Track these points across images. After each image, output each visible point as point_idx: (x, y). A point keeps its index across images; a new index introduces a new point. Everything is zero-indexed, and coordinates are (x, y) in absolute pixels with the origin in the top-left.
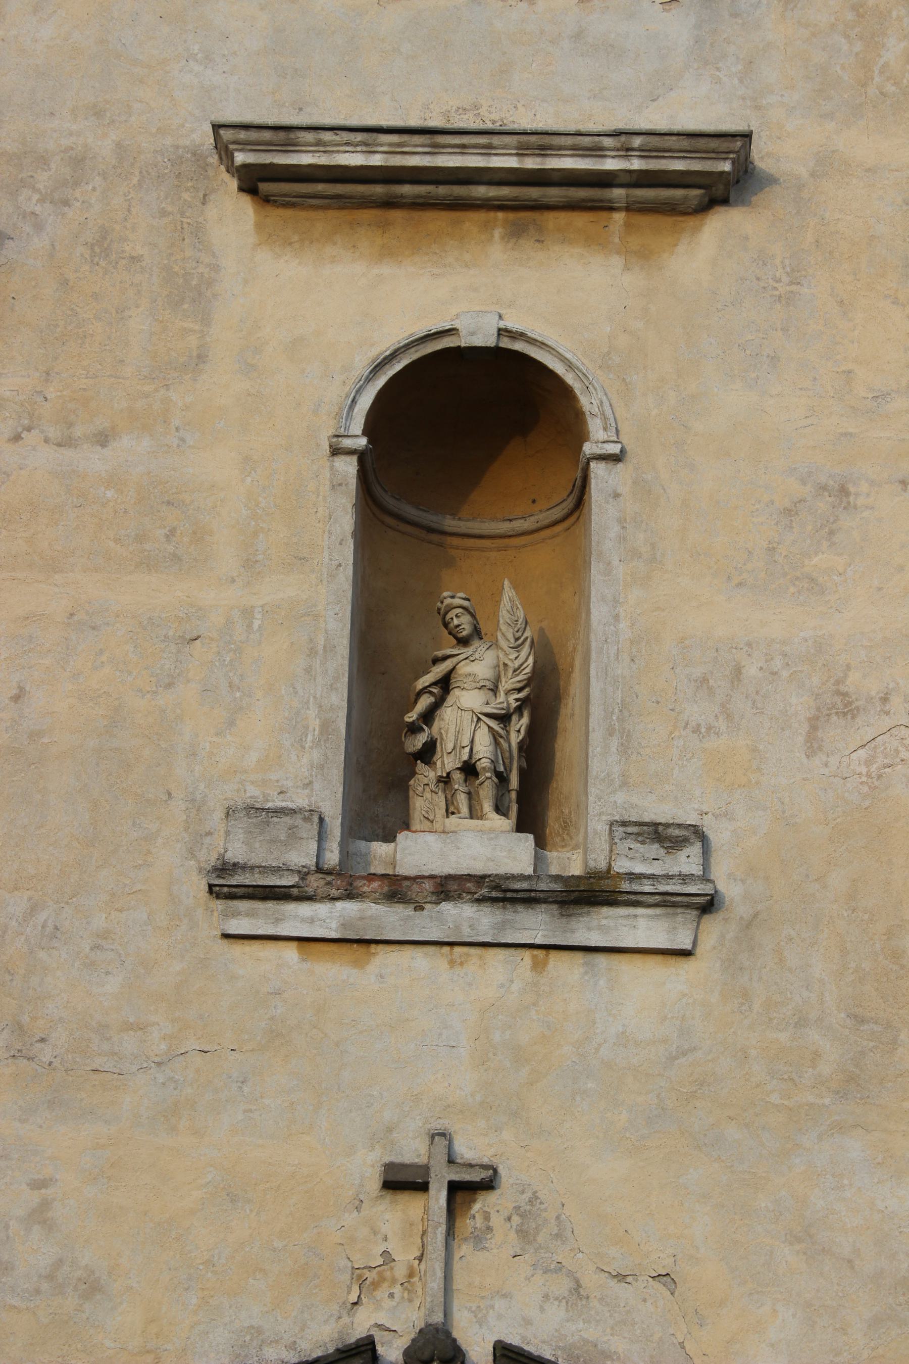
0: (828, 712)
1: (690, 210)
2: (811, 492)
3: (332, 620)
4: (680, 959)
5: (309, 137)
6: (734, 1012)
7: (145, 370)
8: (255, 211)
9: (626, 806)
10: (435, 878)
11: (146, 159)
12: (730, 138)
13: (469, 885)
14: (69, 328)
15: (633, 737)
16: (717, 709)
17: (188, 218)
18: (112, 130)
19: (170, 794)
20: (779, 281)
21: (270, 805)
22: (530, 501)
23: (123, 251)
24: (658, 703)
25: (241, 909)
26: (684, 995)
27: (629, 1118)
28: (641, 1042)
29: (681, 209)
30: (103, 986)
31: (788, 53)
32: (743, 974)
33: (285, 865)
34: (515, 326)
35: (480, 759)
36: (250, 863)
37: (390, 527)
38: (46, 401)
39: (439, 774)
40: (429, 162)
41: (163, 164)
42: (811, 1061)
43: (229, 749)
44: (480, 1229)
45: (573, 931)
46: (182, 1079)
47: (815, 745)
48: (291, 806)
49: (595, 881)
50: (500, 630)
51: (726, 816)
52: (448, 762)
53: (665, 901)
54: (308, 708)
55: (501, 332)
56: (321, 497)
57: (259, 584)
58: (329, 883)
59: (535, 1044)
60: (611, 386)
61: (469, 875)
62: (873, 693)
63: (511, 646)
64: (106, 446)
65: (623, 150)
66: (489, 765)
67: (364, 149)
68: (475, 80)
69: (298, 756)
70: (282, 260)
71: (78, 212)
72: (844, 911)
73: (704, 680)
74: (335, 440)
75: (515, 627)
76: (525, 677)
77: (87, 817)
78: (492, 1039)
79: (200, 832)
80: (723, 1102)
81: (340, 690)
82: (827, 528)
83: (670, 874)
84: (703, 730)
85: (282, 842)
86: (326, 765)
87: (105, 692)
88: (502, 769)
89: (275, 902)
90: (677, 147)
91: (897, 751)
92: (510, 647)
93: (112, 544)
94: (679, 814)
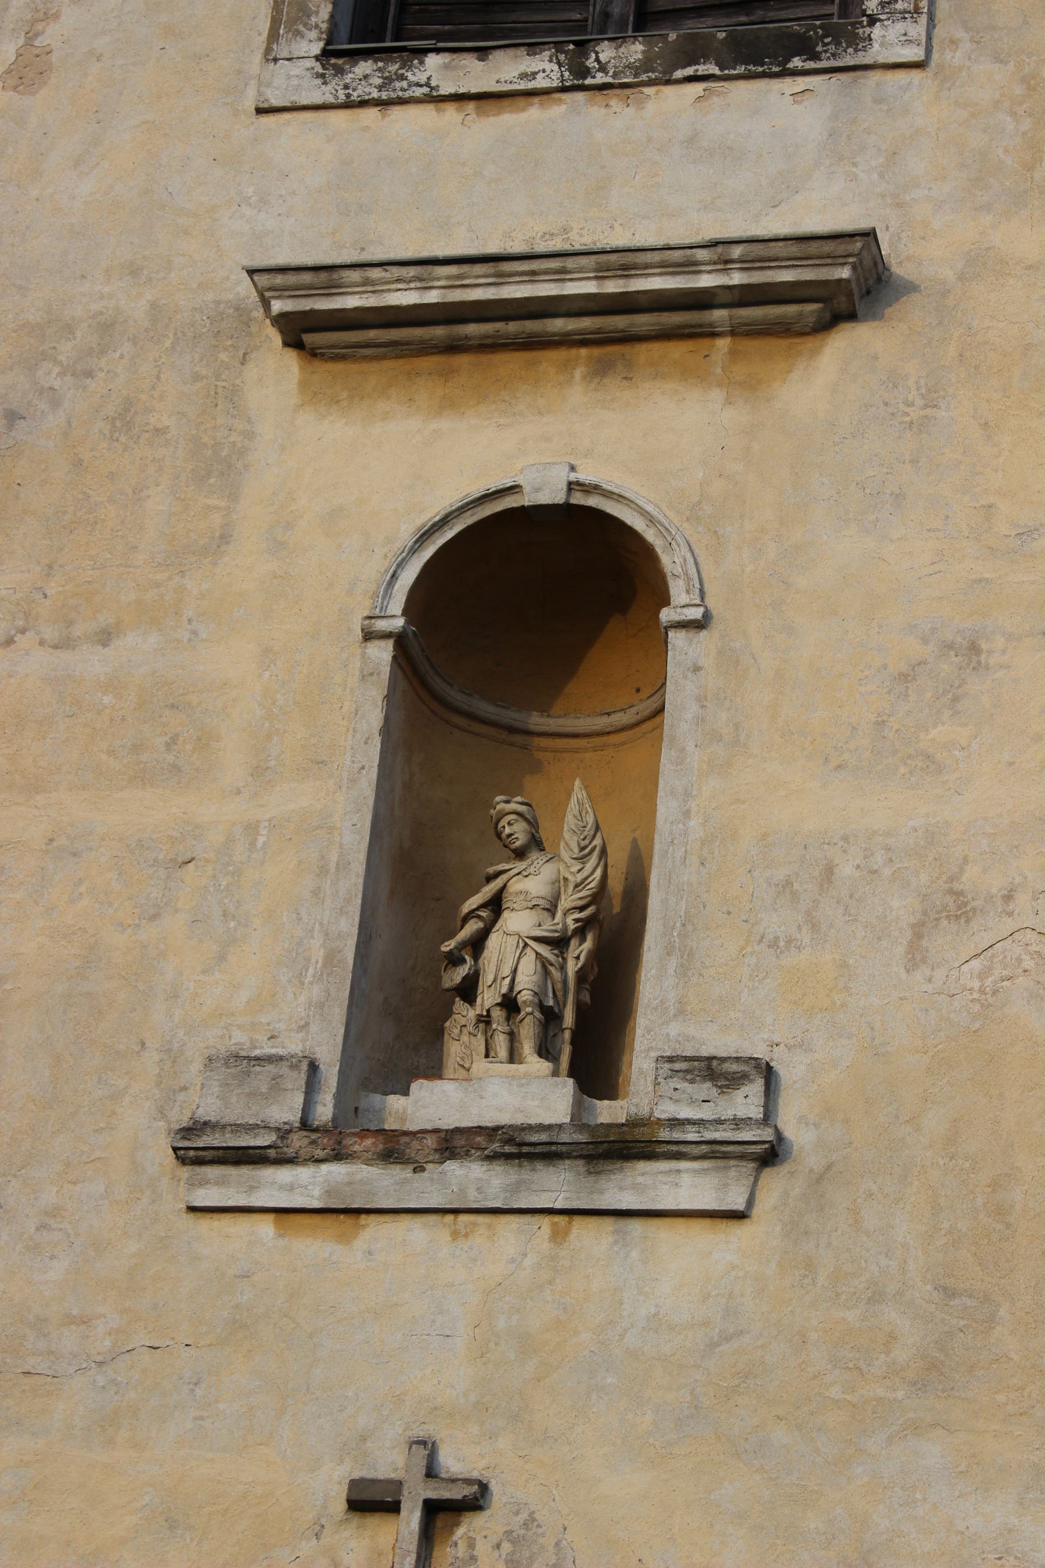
0: (937, 916)
1: (808, 330)
2: (933, 652)
3: (348, 832)
4: (732, 1223)
5: (355, 275)
6: (793, 1286)
7: (159, 556)
8: (301, 368)
9: (680, 1039)
10: (440, 1132)
11: (183, 318)
12: (847, 239)
13: (478, 1139)
14: (79, 514)
15: (696, 956)
16: (800, 918)
17: (223, 381)
18: (149, 289)
19: (143, 1044)
20: (912, 404)
21: (257, 1052)
22: (634, 690)
23: (147, 423)
24: (729, 913)
25: (210, 1176)
26: (734, 1268)
27: (654, 1420)
28: (677, 1325)
29: (797, 329)
30: (46, 1272)
31: (940, 139)
32: (808, 1239)
33: (264, 1122)
34: (588, 478)
35: (520, 991)
36: (223, 1121)
37: (458, 728)
38: (45, 598)
39: (478, 1012)
40: (493, 294)
41: (202, 322)
42: (884, 1344)
43: (216, 988)
44: (462, 1559)
45: (601, 1192)
46: (126, 1381)
47: (918, 957)
48: (281, 1053)
49: (627, 1129)
50: (564, 838)
51: (801, 1047)
52: (488, 997)
53: (713, 1152)
54: (312, 937)
55: (572, 486)
56: (348, 690)
57: (268, 794)
58: (313, 1142)
59: (548, 1331)
60: (700, 541)
61: (479, 1127)
62: (994, 891)
63: (574, 857)
64: (108, 645)
65: (720, 263)
66: (531, 998)
67: (419, 285)
68: (567, 201)
69: (295, 994)
70: (327, 421)
71: (101, 383)
72: (940, 1159)
73: (788, 883)
74: (367, 622)
75: (581, 834)
76: (589, 893)
77: (47, 1074)
78: (495, 1326)
79: (174, 1087)
80: (771, 1398)
81: (351, 913)
82: (951, 694)
83: (723, 1118)
84: (782, 944)
85: (263, 1095)
86: (326, 1003)
87: (80, 928)
88: (551, 1002)
89: (251, 1167)
90: (784, 254)
91: (1019, 960)
92: (574, 859)
93: (104, 757)
94: (745, 1046)
